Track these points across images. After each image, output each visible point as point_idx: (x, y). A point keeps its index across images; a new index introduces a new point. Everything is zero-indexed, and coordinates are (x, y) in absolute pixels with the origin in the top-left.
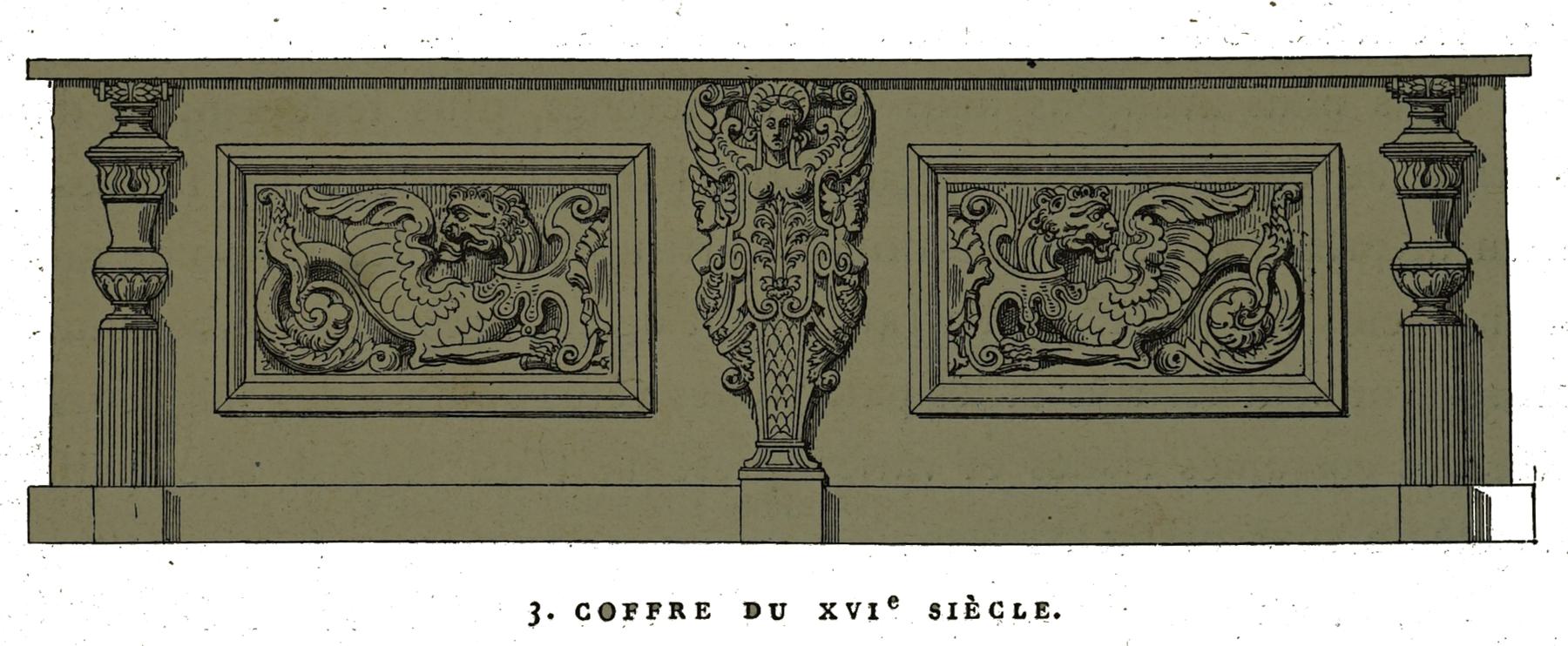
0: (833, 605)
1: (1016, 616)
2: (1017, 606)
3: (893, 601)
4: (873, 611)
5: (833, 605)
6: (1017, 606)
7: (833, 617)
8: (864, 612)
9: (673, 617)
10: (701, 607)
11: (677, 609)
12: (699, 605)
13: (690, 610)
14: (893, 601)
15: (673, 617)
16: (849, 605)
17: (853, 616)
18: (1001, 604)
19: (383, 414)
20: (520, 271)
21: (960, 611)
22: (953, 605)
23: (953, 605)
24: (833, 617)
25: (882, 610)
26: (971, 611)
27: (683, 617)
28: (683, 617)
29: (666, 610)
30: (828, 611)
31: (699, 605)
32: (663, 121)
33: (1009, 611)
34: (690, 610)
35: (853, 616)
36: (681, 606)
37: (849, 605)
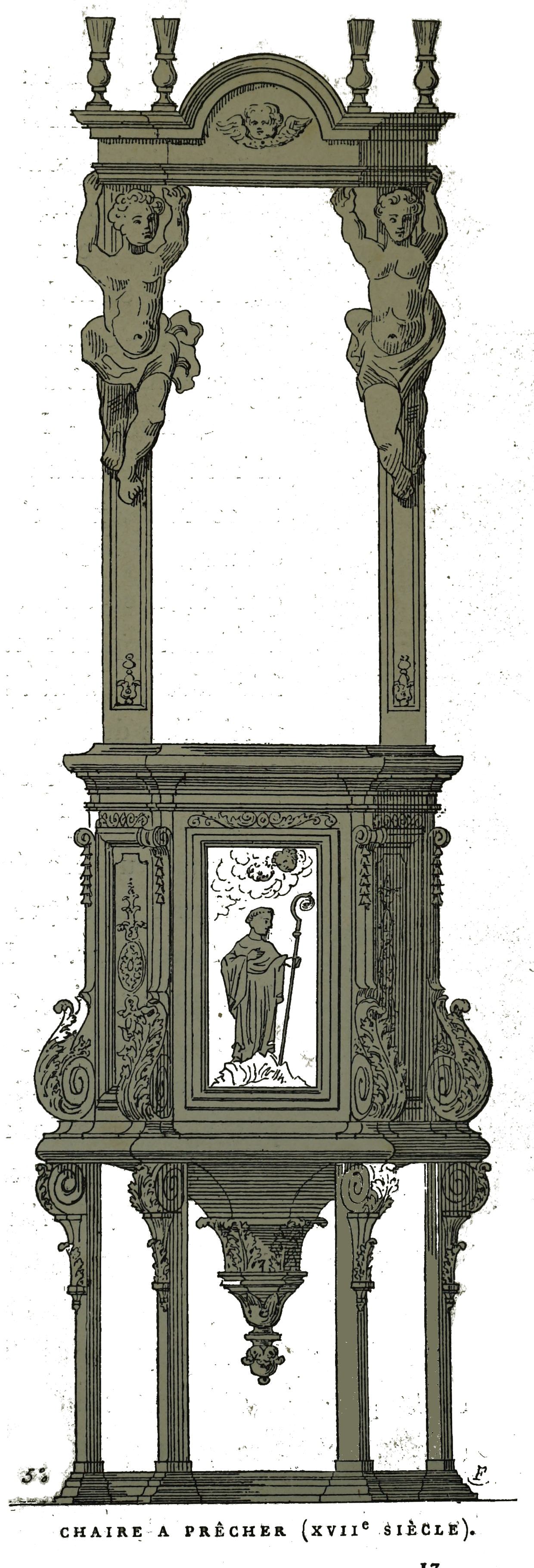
0: (320, 1527)
1: (437, 1533)
2: (438, 1527)
3: (365, 1524)
4: (109, 1533)
5: (320, 1527)
6: (438, 1527)
7: (320, 1535)
8: (338, 1531)
9: (202, 1535)
10: (136, 1529)
11: (265, 1531)
12: (134, 1528)
13: (130, 1532)
14: (365, 1524)
15: (202, 1535)
16: (329, 1527)
17: (331, 1534)
18: (236, 1528)
19: (339, 887)
20: (344, 188)
21: (405, 1530)
22: (399, 1527)
23: (399, 1527)
24: (320, 1535)
25: (360, 1529)
26: (265, 1531)
27: (126, 1536)
28: (126, 1536)
29: (198, 1531)
30: (317, 1531)
31: (134, 1528)
32: (100, 22)
33: (433, 1530)
34: (130, 1532)
35: (331, 1534)
36: (206, 1529)
37: (329, 1527)
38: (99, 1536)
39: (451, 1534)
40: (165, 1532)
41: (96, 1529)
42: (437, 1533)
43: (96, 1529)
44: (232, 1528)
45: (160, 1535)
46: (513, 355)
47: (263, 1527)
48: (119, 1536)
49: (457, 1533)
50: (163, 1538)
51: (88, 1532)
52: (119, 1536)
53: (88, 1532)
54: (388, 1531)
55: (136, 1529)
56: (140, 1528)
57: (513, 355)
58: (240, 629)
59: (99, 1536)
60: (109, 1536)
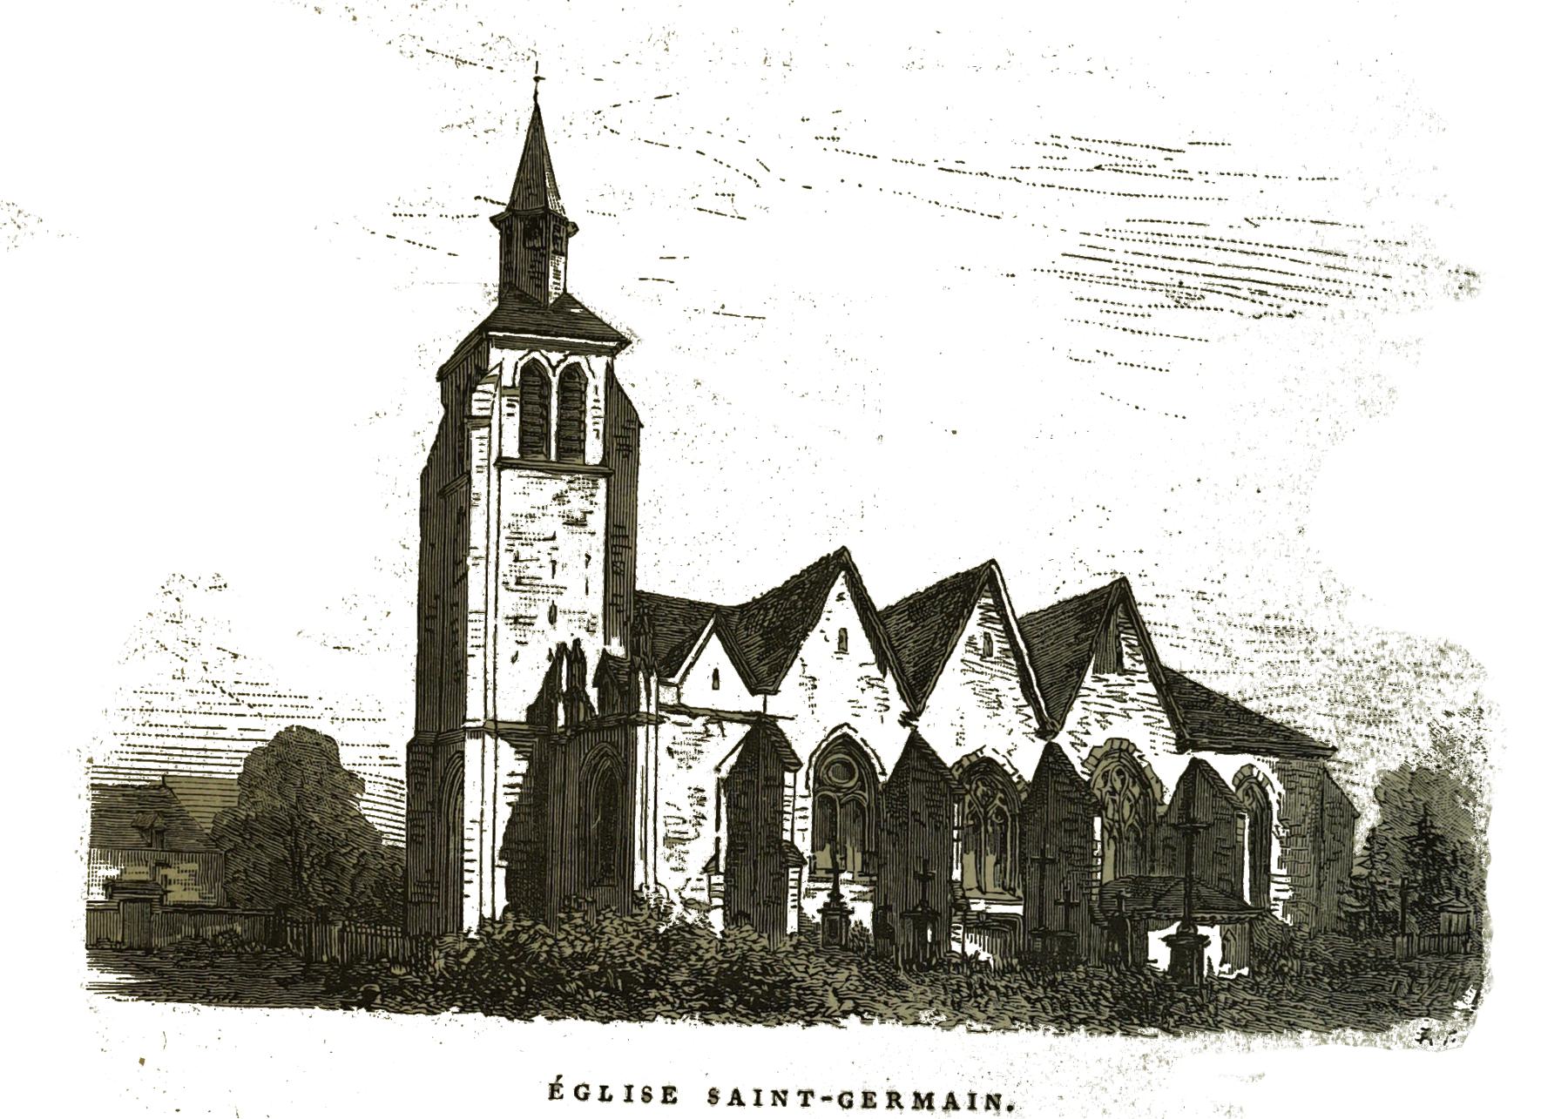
1: (602, 1099)
2: (604, 1088)
6: (604, 1088)
10: (668, 1091)
18: (851, 1094)
31: (665, 1089)
38: (741, 1104)
39: (665, 1101)
40: (739, 1098)
41: (736, 1091)
42: (602, 1099)
43: (736, 1091)
44: (577, 1089)
45: (731, 1104)
46: (395, 47)
47: (865, 1094)
48: (890, 1106)
49: (675, 1101)
50: (735, 1107)
51: (940, 1101)
52: (890, 1106)
53: (940, 1101)
54: (554, 1090)
55: (668, 1091)
56: (674, 1089)
57: (395, 47)
58: (685, 348)
59: (741, 1104)
60: (758, 1103)
